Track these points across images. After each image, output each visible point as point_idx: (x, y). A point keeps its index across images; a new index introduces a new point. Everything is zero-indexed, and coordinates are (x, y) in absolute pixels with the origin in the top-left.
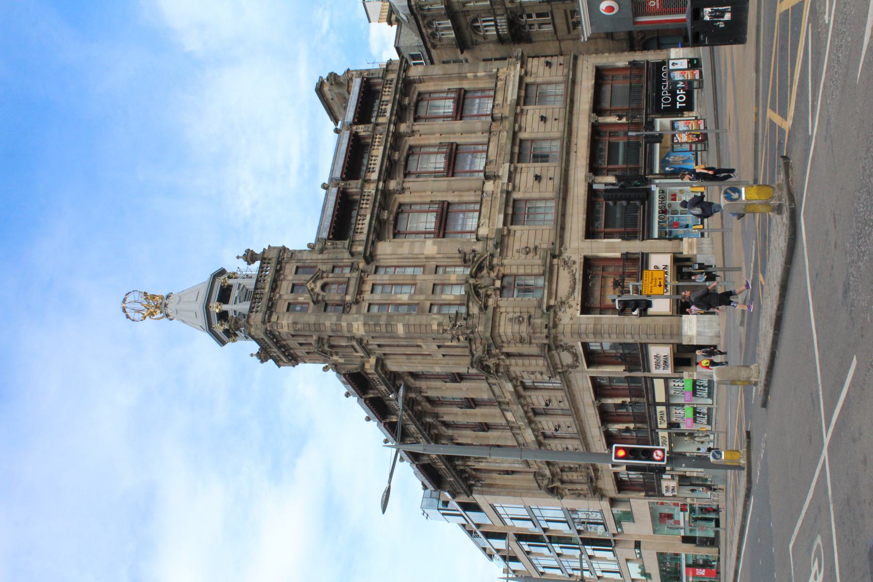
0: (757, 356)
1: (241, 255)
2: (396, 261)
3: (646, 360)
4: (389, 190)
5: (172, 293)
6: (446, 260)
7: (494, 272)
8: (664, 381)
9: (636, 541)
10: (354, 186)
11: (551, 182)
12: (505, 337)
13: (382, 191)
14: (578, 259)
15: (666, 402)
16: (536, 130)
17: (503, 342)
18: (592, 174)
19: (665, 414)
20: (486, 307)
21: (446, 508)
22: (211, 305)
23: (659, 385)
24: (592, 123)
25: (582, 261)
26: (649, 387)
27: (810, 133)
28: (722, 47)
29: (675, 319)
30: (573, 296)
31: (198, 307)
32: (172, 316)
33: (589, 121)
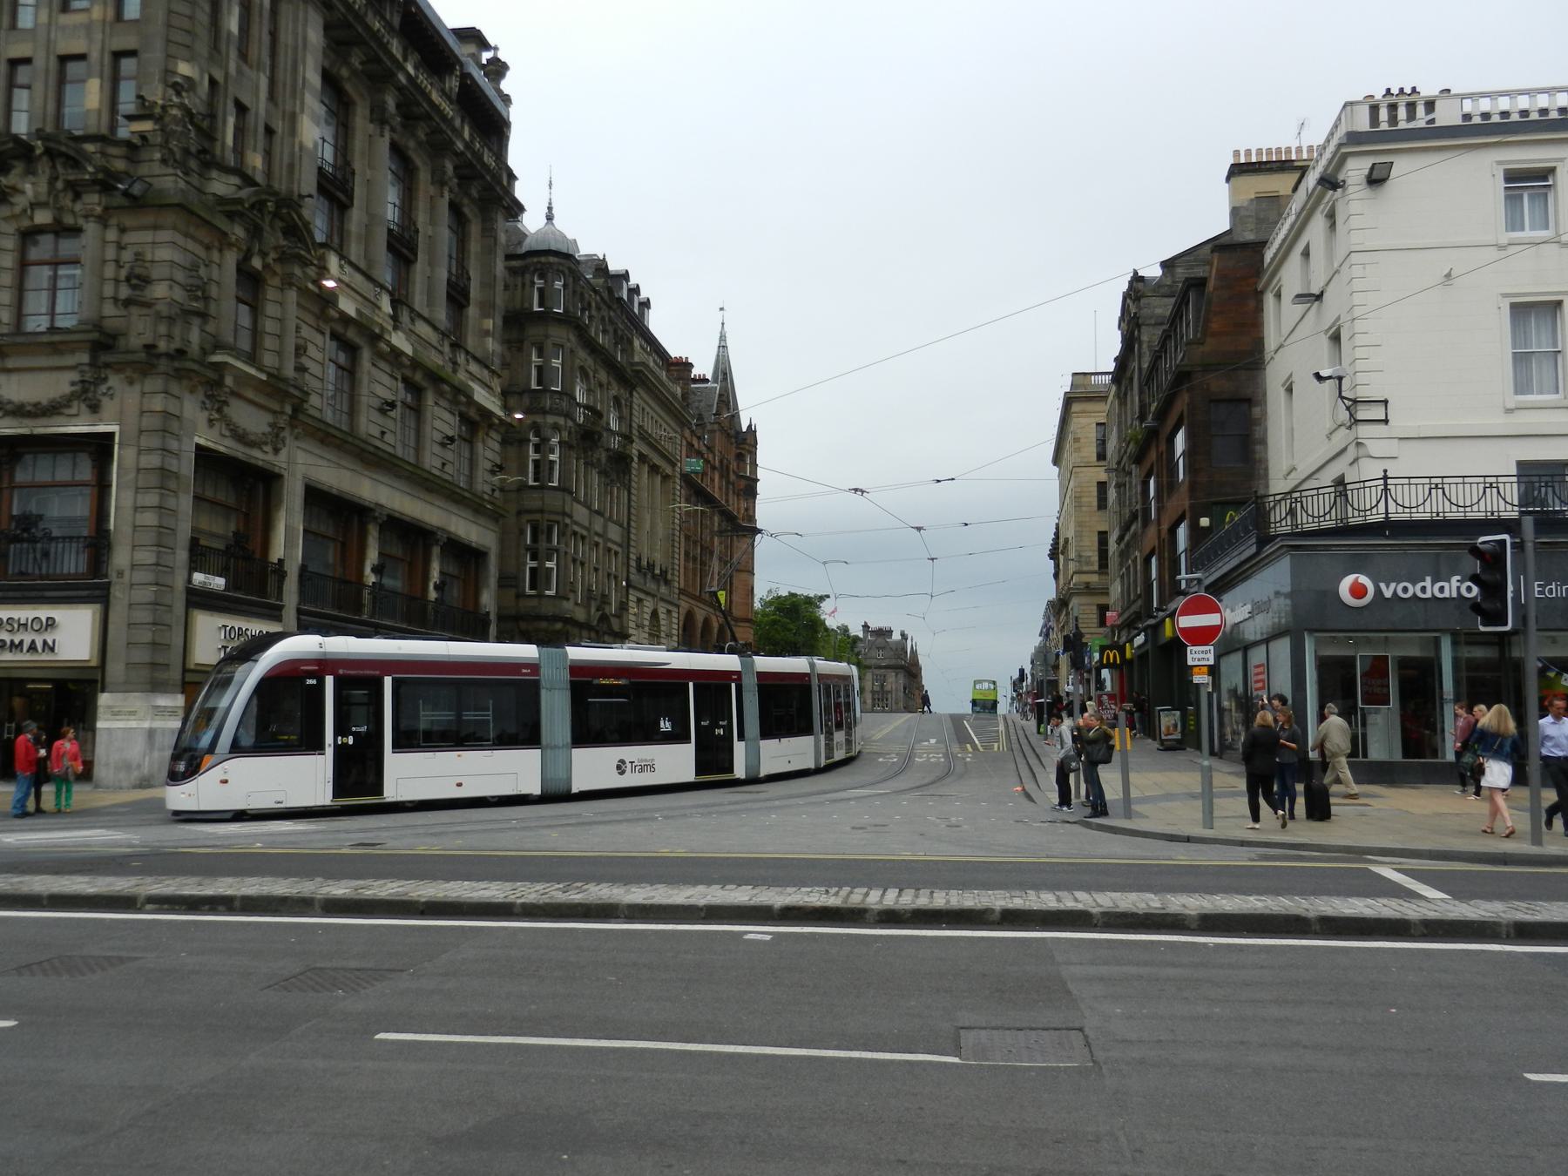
0: (779, 889)
2: (290, 41)
3: (18, 594)
6: (286, 160)
7: (274, 260)
9: (1100, 533)
11: (376, 433)
14: (279, 461)
17: (123, 230)
18: (385, 519)
20: (230, 216)
25: (277, 470)
27: (768, 937)
28: (1245, 780)
29: (175, 674)
30: (228, 434)
33: (438, 528)
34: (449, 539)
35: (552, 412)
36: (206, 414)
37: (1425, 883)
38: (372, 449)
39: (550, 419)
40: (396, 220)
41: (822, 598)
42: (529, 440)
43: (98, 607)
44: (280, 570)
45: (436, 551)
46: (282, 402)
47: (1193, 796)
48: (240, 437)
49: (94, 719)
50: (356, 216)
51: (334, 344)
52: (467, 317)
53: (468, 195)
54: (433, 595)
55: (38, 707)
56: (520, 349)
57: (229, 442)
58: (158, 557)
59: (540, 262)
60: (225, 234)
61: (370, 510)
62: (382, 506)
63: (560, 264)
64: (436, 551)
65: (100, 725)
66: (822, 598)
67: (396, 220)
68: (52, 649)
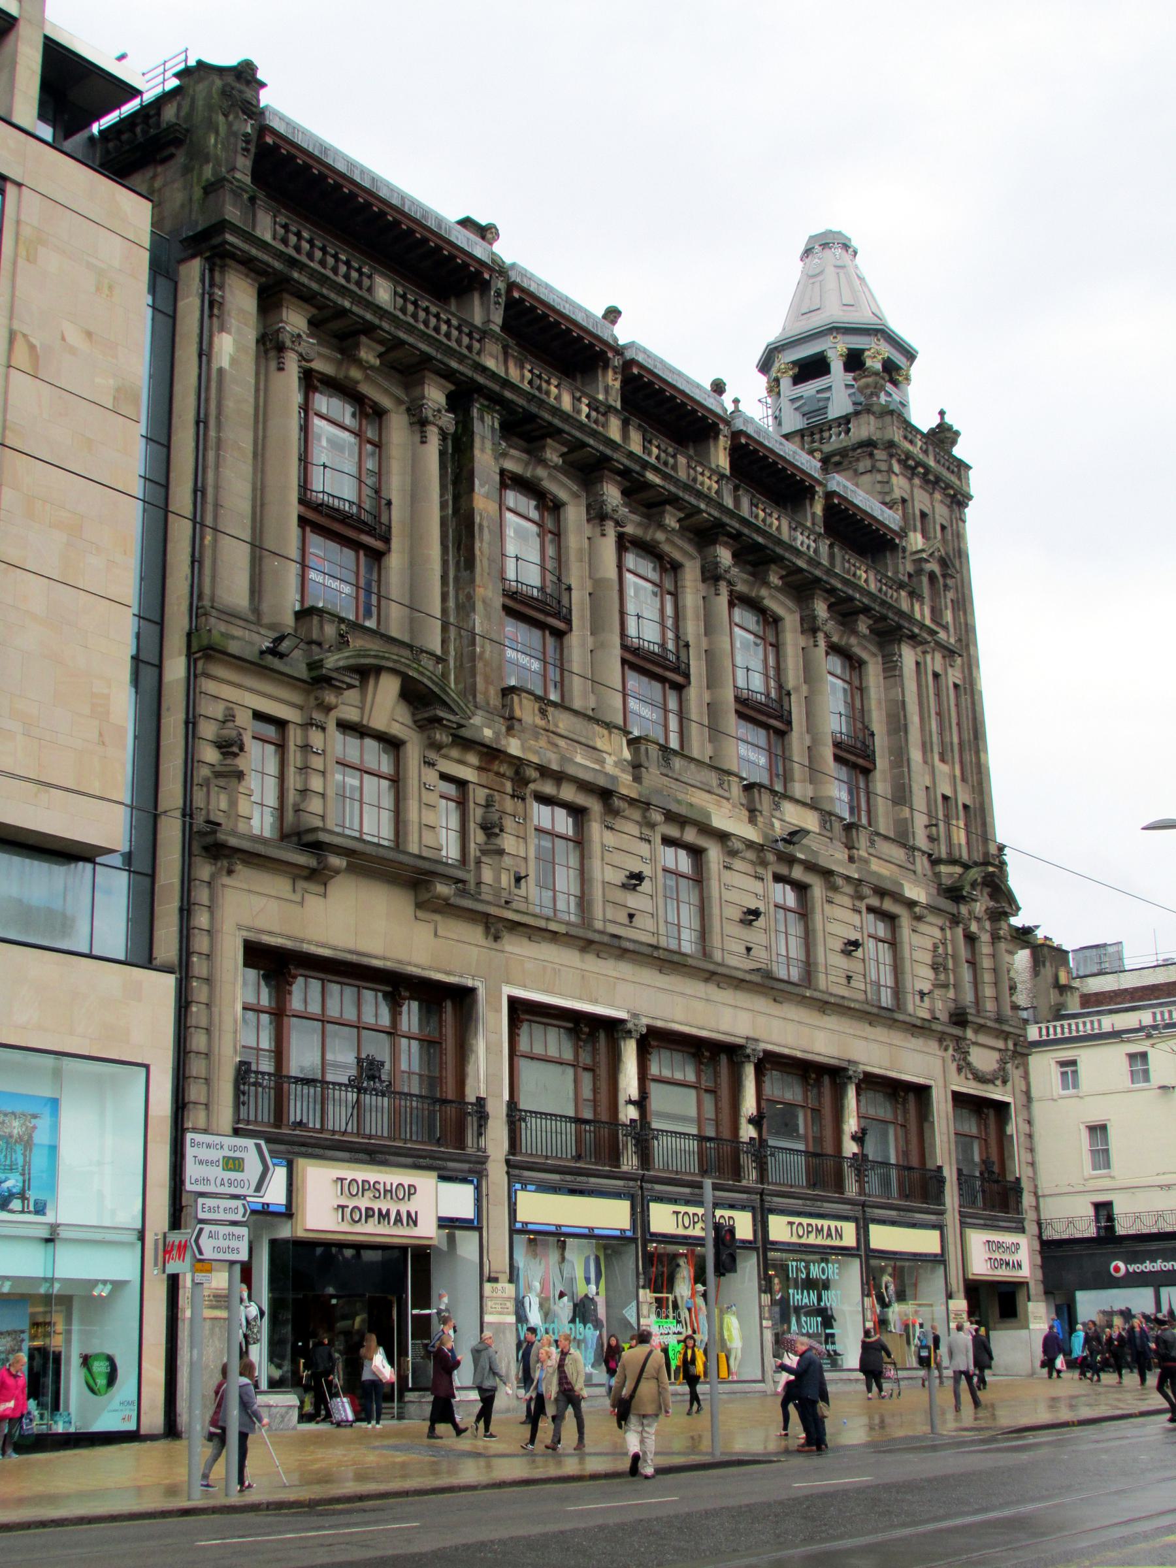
1: (948, 419)
4: (600, 480)
5: (855, 253)
8: (936, 1255)
10: (610, 385)
12: (791, 931)
13: (900, 627)
15: (858, 1248)
16: (727, 895)
19: (829, 1242)
21: (231, 705)
22: (839, 337)
23: (924, 1241)
24: (845, 1069)
26: (593, 1180)
31: (833, 313)
32: (814, 260)
38: (606, 939)
40: (844, 730)
41: (1037, 927)
44: (480, 1107)
45: (851, 1092)
46: (1006, 1040)
47: (1044, 1196)
48: (980, 1078)
50: (798, 739)
51: (871, 917)
53: (359, 363)
55: (331, 1290)
57: (973, 1084)
61: (741, 1047)
62: (855, 1063)
64: (851, 1092)
66: (1037, 927)
67: (844, 730)
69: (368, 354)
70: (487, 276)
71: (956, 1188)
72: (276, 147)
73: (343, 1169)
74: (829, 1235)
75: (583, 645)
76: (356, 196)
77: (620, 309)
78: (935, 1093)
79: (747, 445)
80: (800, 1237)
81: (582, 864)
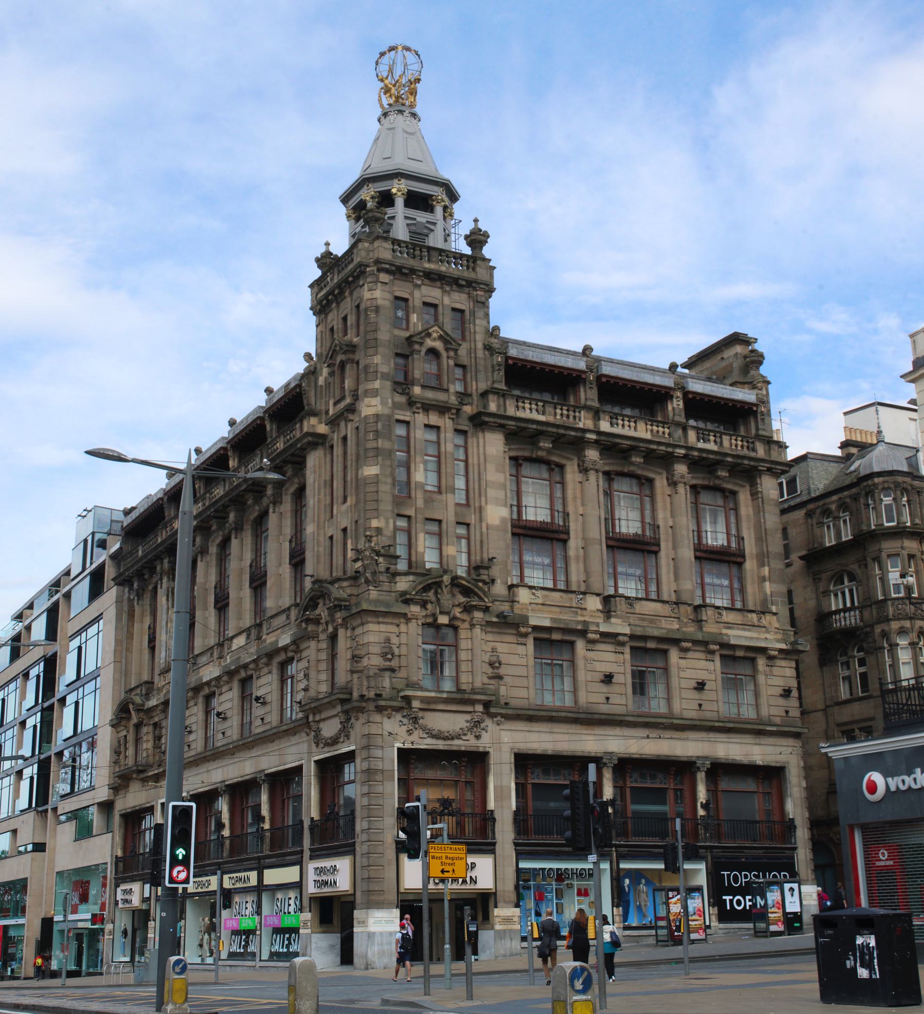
2: (476, 462)
3: (329, 852)
4: (584, 450)
7: (460, 613)
10: (588, 395)
14: (485, 742)
16: (682, 674)
17: (353, 629)
18: (616, 762)
20: (407, 602)
25: (481, 750)
29: (393, 897)
30: (426, 736)
33: (698, 757)
34: (712, 764)
35: (897, 618)
36: (405, 728)
37: (353, 958)
39: (895, 625)
42: (884, 648)
43: (350, 857)
49: (352, 927)
52: (745, 569)
54: (701, 812)
56: (866, 566)
57: (430, 741)
58: (369, 824)
59: (868, 485)
60: (406, 614)
63: (884, 482)
65: (355, 930)
68: (476, 882)
69: (546, 444)
70: (755, 409)
71: (309, 833)
72: (608, 382)
73: (638, 863)
74: (464, 882)
75: (668, 557)
76: (635, 386)
77: (593, 347)
78: (493, 759)
79: (694, 398)
80: (233, 884)
81: (574, 674)
